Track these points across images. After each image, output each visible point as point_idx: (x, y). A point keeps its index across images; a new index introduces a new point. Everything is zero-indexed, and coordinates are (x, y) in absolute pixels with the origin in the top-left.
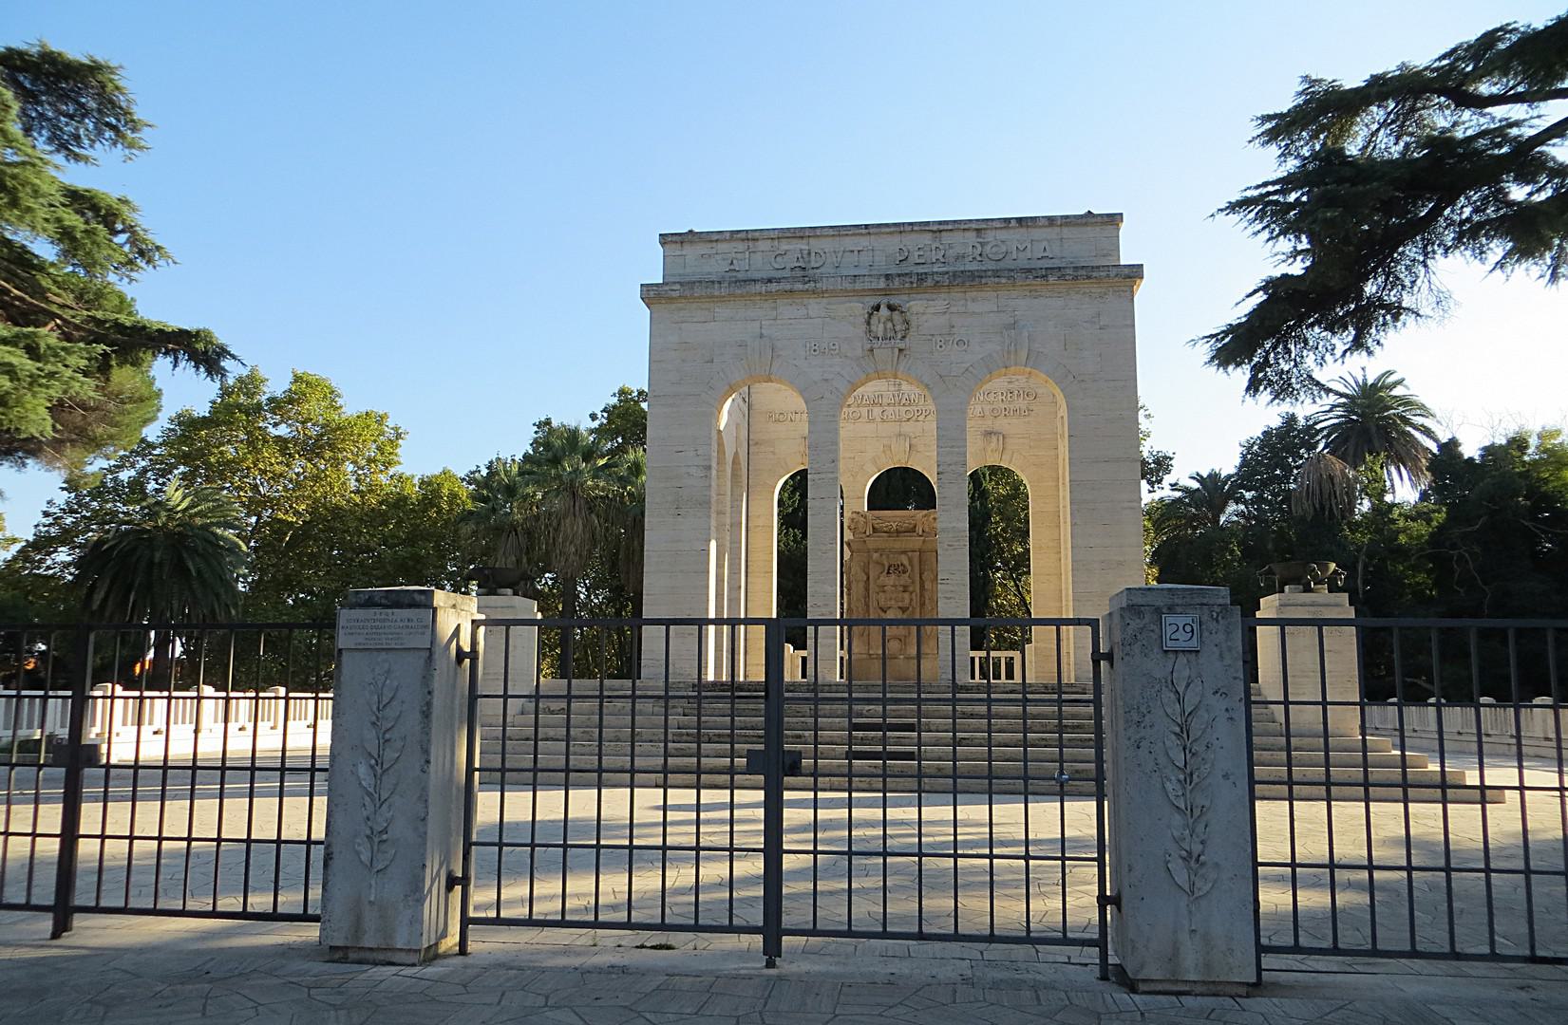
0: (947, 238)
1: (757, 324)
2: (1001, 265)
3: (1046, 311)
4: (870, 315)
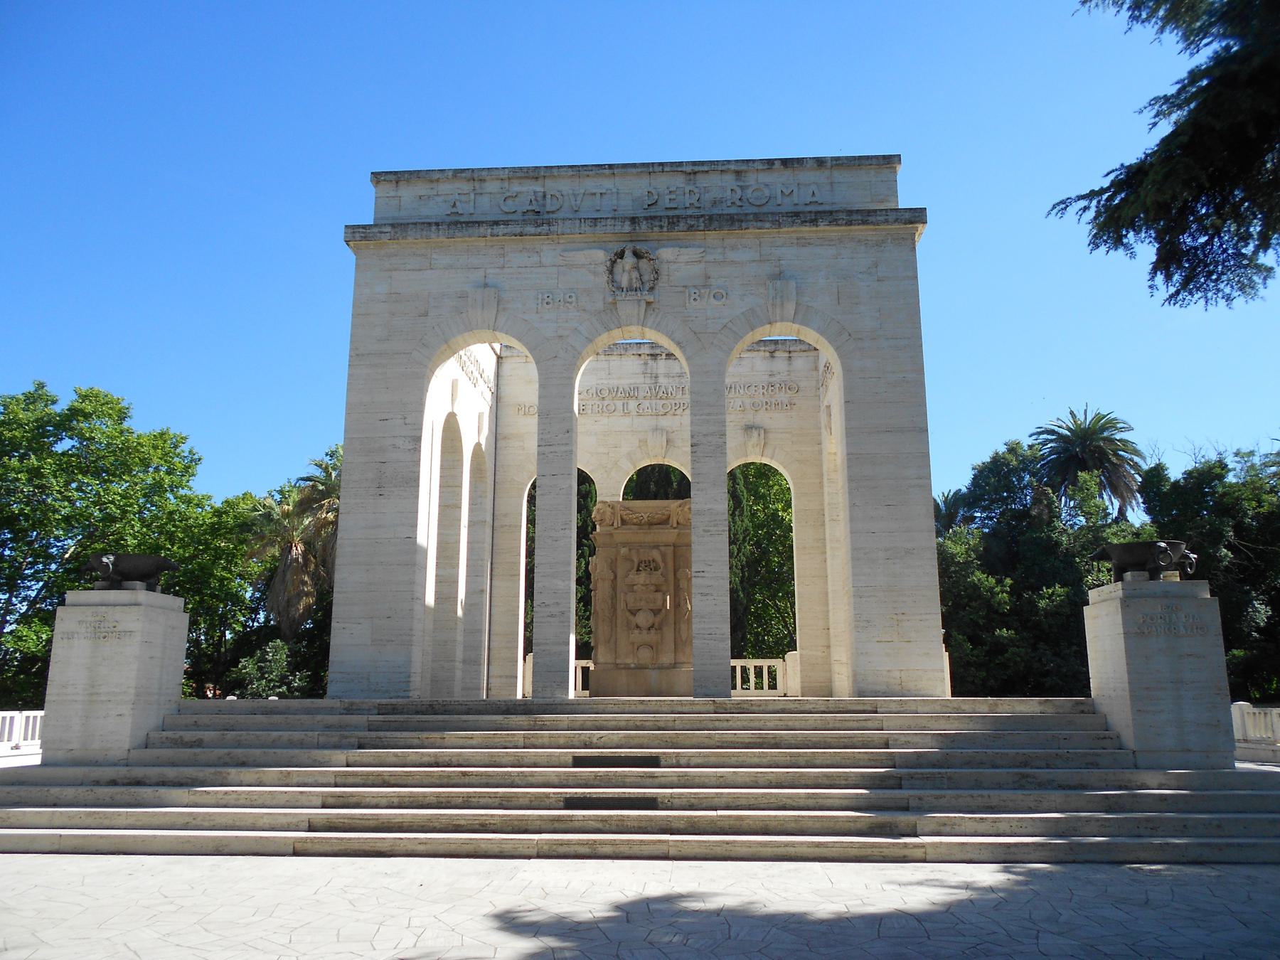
0: (702, 181)
1: (481, 273)
2: (765, 209)
3: (817, 255)
4: (613, 262)
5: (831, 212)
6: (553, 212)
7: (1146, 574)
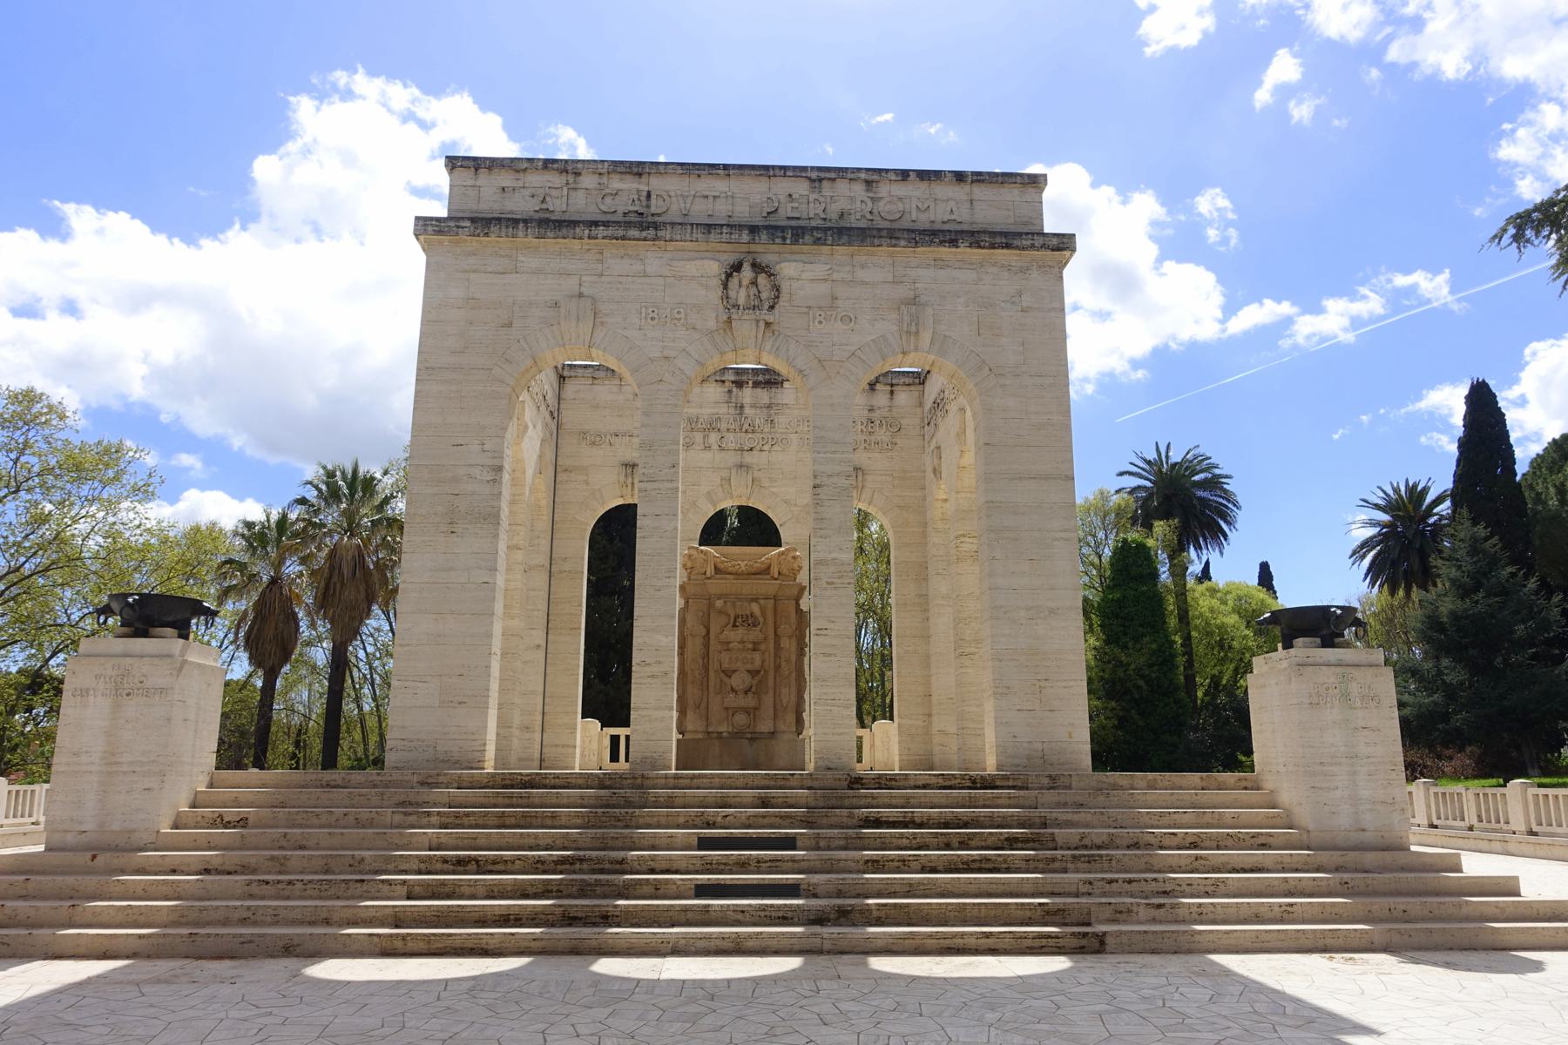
1: (574, 280)
4: (729, 276)
5: (972, 233)
6: (659, 215)
7: (1318, 640)
